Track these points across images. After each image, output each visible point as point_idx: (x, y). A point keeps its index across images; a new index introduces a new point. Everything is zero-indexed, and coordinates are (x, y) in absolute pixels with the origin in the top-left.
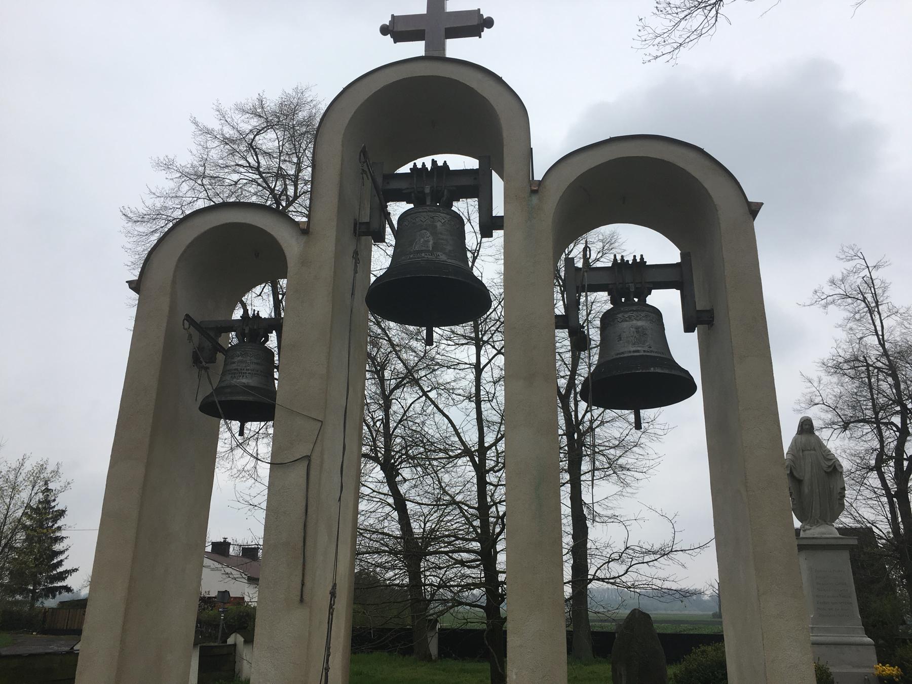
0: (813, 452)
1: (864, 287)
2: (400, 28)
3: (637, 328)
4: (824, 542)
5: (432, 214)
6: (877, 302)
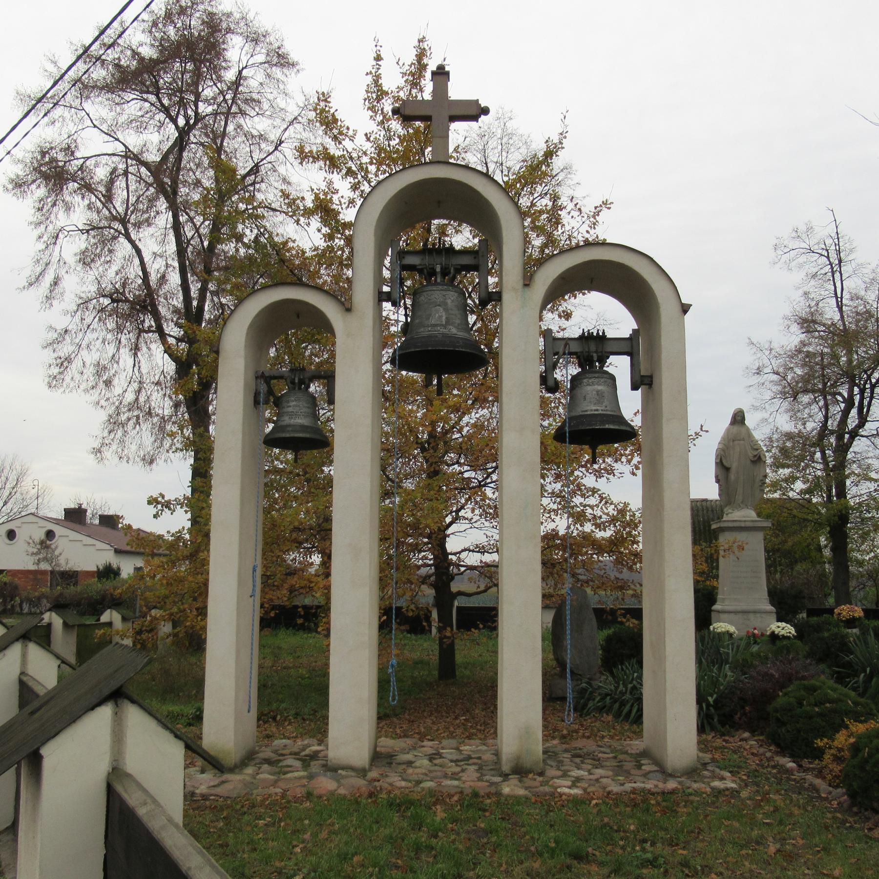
0: (742, 442)
1: (829, 242)
2: (408, 112)
3: (598, 392)
4: (743, 525)
5: (444, 293)
6: (840, 261)
